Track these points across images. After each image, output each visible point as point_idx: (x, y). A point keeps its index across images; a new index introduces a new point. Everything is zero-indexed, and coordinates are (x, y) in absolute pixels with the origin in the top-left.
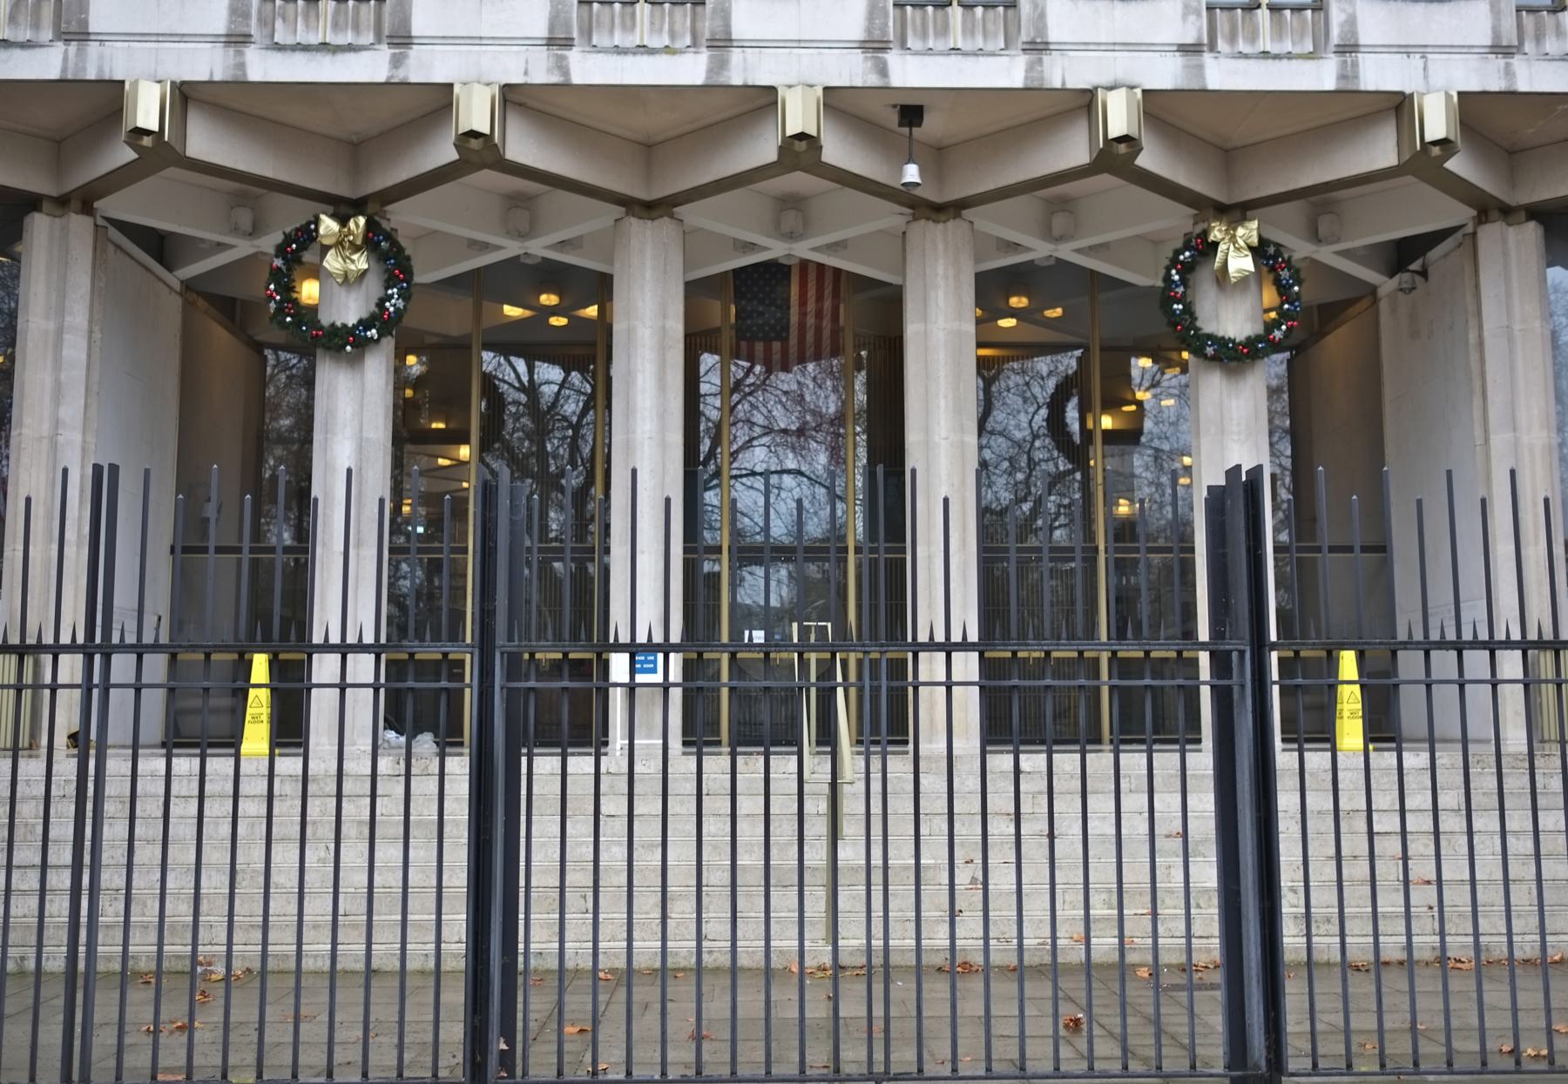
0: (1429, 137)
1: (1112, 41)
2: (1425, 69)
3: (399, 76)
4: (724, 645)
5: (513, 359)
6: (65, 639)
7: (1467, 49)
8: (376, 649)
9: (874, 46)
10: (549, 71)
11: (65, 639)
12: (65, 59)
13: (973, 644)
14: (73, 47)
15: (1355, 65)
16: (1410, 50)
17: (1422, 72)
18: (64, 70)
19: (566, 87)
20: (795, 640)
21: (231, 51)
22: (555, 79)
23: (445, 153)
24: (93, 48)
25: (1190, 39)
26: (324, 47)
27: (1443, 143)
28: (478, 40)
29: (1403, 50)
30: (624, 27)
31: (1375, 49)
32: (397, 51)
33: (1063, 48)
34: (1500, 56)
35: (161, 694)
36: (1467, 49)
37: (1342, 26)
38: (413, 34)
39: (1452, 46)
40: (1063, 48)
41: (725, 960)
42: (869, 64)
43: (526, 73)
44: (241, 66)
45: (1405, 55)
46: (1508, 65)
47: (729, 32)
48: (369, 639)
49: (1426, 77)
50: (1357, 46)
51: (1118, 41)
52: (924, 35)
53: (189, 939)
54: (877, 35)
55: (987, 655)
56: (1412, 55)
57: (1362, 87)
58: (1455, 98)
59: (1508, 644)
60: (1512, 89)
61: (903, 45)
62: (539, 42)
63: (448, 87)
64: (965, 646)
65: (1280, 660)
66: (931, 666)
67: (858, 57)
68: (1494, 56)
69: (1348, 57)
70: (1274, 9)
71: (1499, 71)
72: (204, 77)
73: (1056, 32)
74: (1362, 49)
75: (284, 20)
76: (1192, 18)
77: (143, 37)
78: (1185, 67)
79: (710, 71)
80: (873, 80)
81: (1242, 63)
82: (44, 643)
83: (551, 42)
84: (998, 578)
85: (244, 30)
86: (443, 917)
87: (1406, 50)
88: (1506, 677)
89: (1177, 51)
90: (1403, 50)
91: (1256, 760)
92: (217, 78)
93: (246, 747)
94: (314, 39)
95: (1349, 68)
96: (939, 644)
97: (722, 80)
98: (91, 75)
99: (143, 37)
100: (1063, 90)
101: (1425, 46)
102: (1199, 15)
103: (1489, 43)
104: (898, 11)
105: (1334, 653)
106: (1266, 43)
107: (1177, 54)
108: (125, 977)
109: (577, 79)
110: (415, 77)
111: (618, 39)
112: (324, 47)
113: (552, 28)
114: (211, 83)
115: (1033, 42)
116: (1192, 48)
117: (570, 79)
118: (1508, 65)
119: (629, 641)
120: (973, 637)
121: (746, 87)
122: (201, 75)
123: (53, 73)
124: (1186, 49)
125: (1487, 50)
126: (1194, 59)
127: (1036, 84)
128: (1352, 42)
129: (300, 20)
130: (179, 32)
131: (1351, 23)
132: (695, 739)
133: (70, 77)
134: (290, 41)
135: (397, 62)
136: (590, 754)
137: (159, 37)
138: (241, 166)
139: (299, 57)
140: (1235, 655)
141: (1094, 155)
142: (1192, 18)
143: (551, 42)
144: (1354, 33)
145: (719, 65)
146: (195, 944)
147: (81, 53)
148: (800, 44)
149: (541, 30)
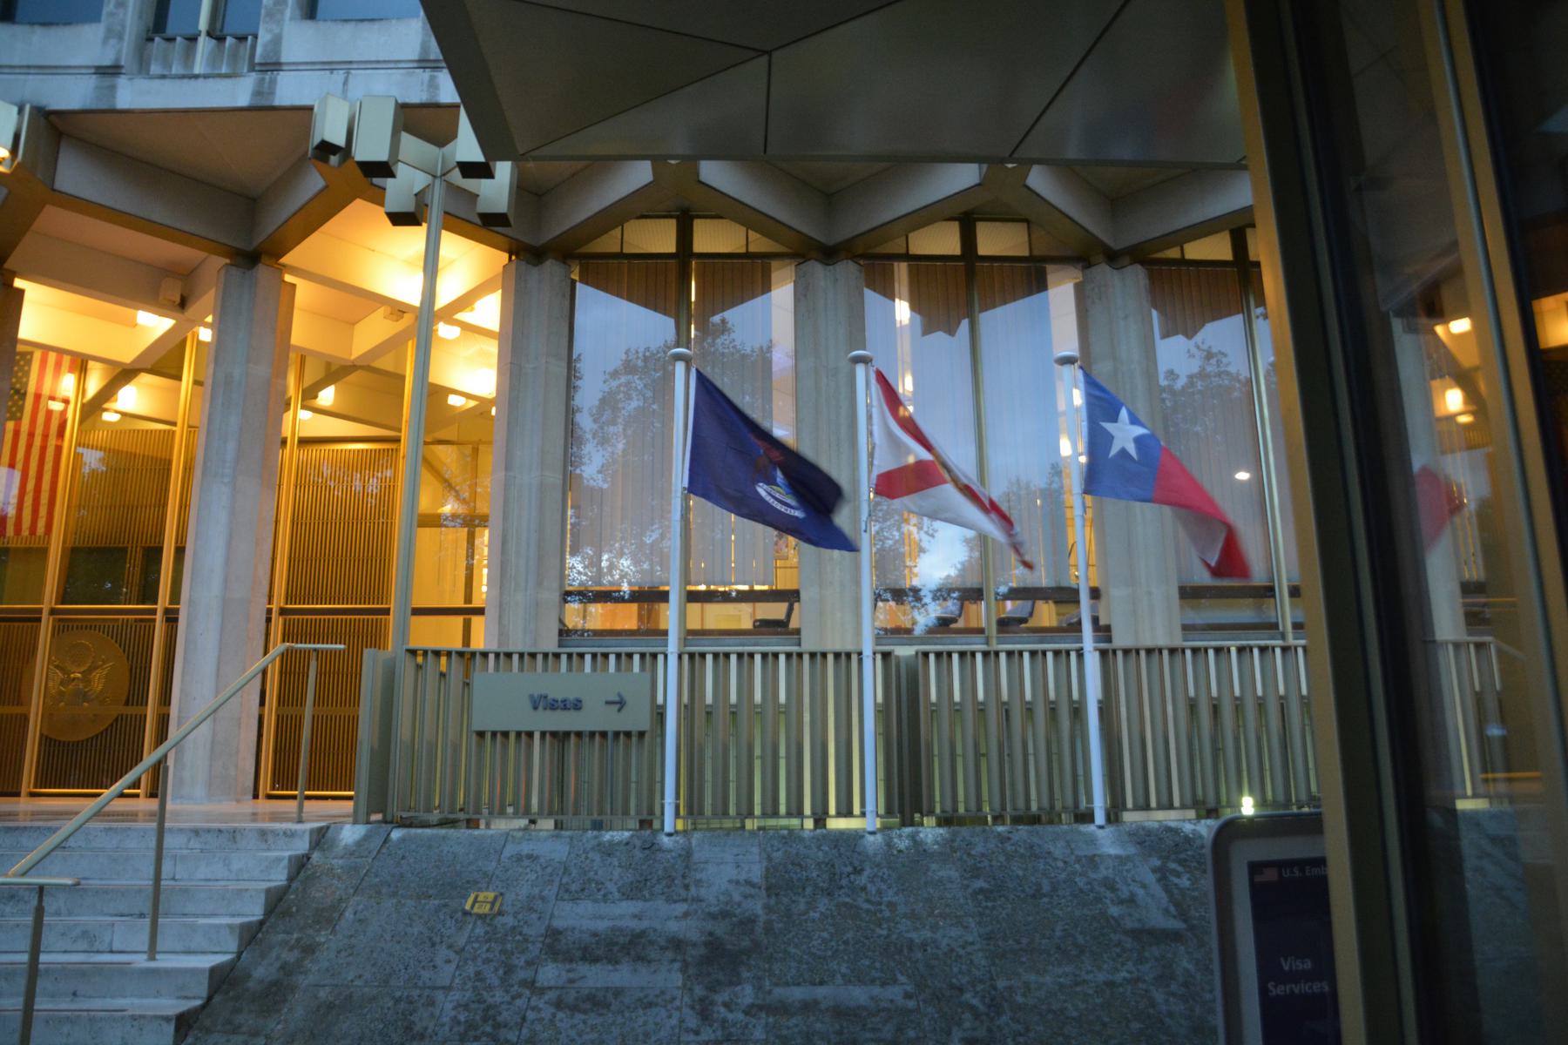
1: (25, 63)
5: (472, 403)
7: (393, 64)
15: (273, 82)
16: (334, 67)
17: (341, 85)
29: (327, 67)
31: (297, 66)
34: (427, 70)
37: (265, 46)
39: (378, 62)
45: (328, 72)
46: (432, 79)
50: (280, 64)
51: (31, 63)
53: (26, 944)
56: (335, 72)
57: (277, 102)
60: (434, 101)
62: (411, 65)
67: (92, 81)
68: (422, 70)
71: (422, 83)
74: (285, 68)
76: (112, 42)
78: (97, 87)
84: (40, 537)
87: (329, 66)
89: (95, 73)
90: (327, 67)
91: (158, 728)
93: (624, 904)
95: (266, 85)
101: (350, 62)
103: (416, 58)
105: (1119, 814)
107: (94, 76)
116: (110, 71)
118: (432, 79)
124: (102, 71)
125: (415, 65)
126: (108, 81)
128: (274, 60)
132: (352, 793)
138: (771, 213)
144: (277, 52)
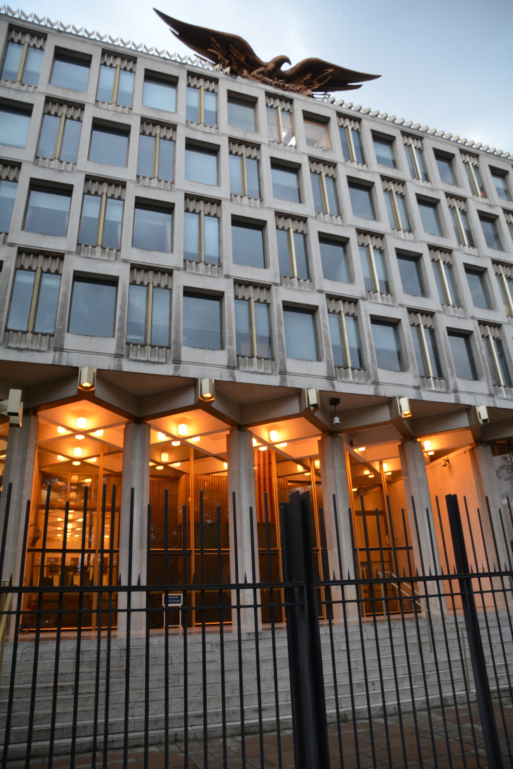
0: (311, 403)
2: (475, 399)
3: (177, 374)
4: (282, 584)
6: (134, 583)
7: (483, 394)
8: (356, 583)
9: (330, 378)
10: (229, 377)
11: (134, 583)
12: (54, 357)
13: (144, 587)
14: (57, 354)
18: (54, 361)
19: (234, 383)
20: (282, 581)
21: (117, 360)
22: (230, 380)
23: (72, 392)
24: (65, 354)
25: (416, 385)
26: (27, 349)
27: (315, 406)
28: (204, 364)
30: (249, 366)
32: (176, 365)
33: (69, 351)
35: (460, 597)
36: (483, 394)
38: (182, 360)
40: (69, 351)
41: (410, 708)
42: (329, 384)
43: (221, 377)
44: (120, 365)
46: (494, 400)
47: (285, 370)
48: (250, 581)
49: (476, 401)
52: (245, 366)
54: (330, 375)
55: (151, 593)
58: (213, 382)
59: (246, 586)
61: (128, 356)
63: (77, 368)
64: (139, 588)
65: (196, 594)
66: (336, 592)
67: (325, 381)
69: (457, 394)
70: (258, 358)
72: (107, 368)
73: (381, 379)
75: (133, 352)
77: (84, 352)
79: (281, 382)
80: (331, 389)
81: (431, 393)
82: (13, 586)
83: (228, 367)
85: (122, 353)
86: (350, 695)
88: (349, 599)
92: (112, 368)
94: (145, 359)
96: (250, 584)
97: (285, 385)
98: (64, 363)
99: (84, 352)
100: (385, 397)
102: (417, 377)
104: (127, 346)
106: (255, 368)
108: (243, 731)
109: (238, 380)
110: (182, 375)
111: (247, 369)
112: (27, 349)
113: (229, 363)
114: (109, 370)
115: (375, 382)
117: (122, 369)
118: (494, 400)
119: (452, 580)
120: (144, 583)
121: (292, 388)
122: (106, 367)
123: (50, 362)
124: (417, 388)
127: (377, 395)
129: (139, 352)
130: (98, 351)
131: (455, 384)
133: (56, 363)
134: (134, 358)
135: (176, 369)
136: (161, 635)
137: (90, 353)
139: (142, 364)
140: (296, 589)
141: (197, 401)
142: (416, 379)
143: (228, 367)
145: (283, 380)
146: (427, 695)
147: (61, 356)
148: (307, 375)
149: (225, 363)
